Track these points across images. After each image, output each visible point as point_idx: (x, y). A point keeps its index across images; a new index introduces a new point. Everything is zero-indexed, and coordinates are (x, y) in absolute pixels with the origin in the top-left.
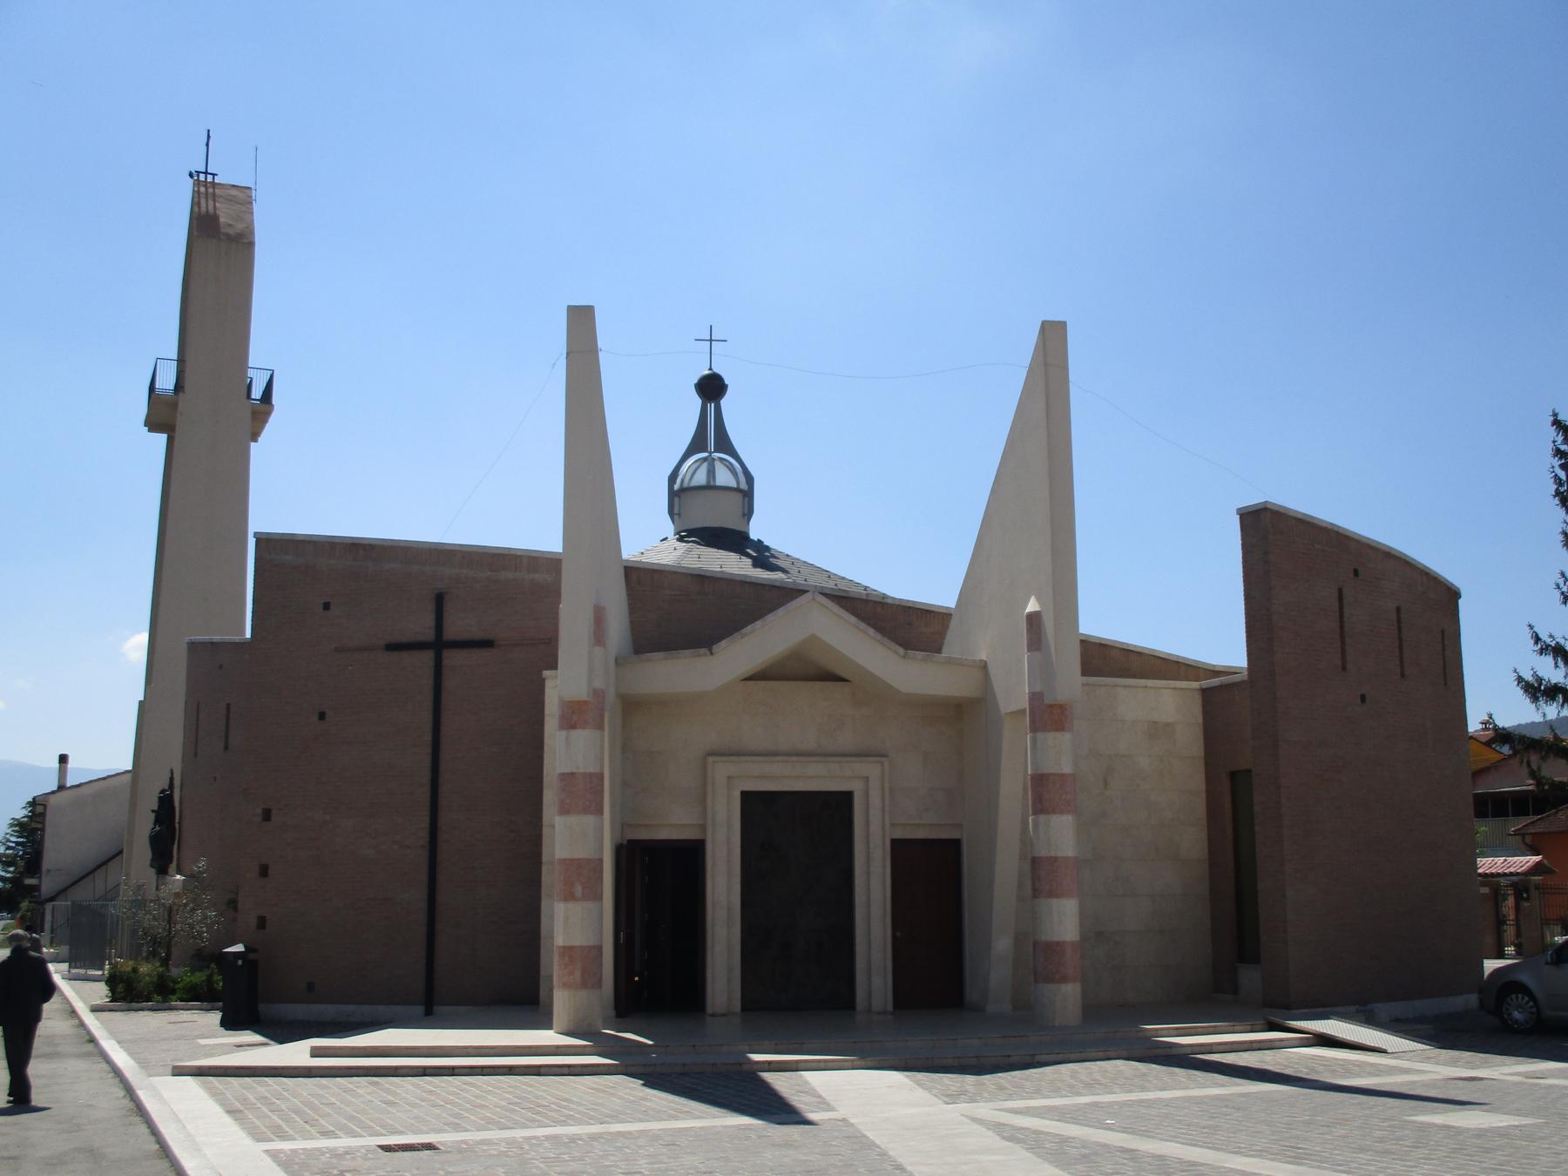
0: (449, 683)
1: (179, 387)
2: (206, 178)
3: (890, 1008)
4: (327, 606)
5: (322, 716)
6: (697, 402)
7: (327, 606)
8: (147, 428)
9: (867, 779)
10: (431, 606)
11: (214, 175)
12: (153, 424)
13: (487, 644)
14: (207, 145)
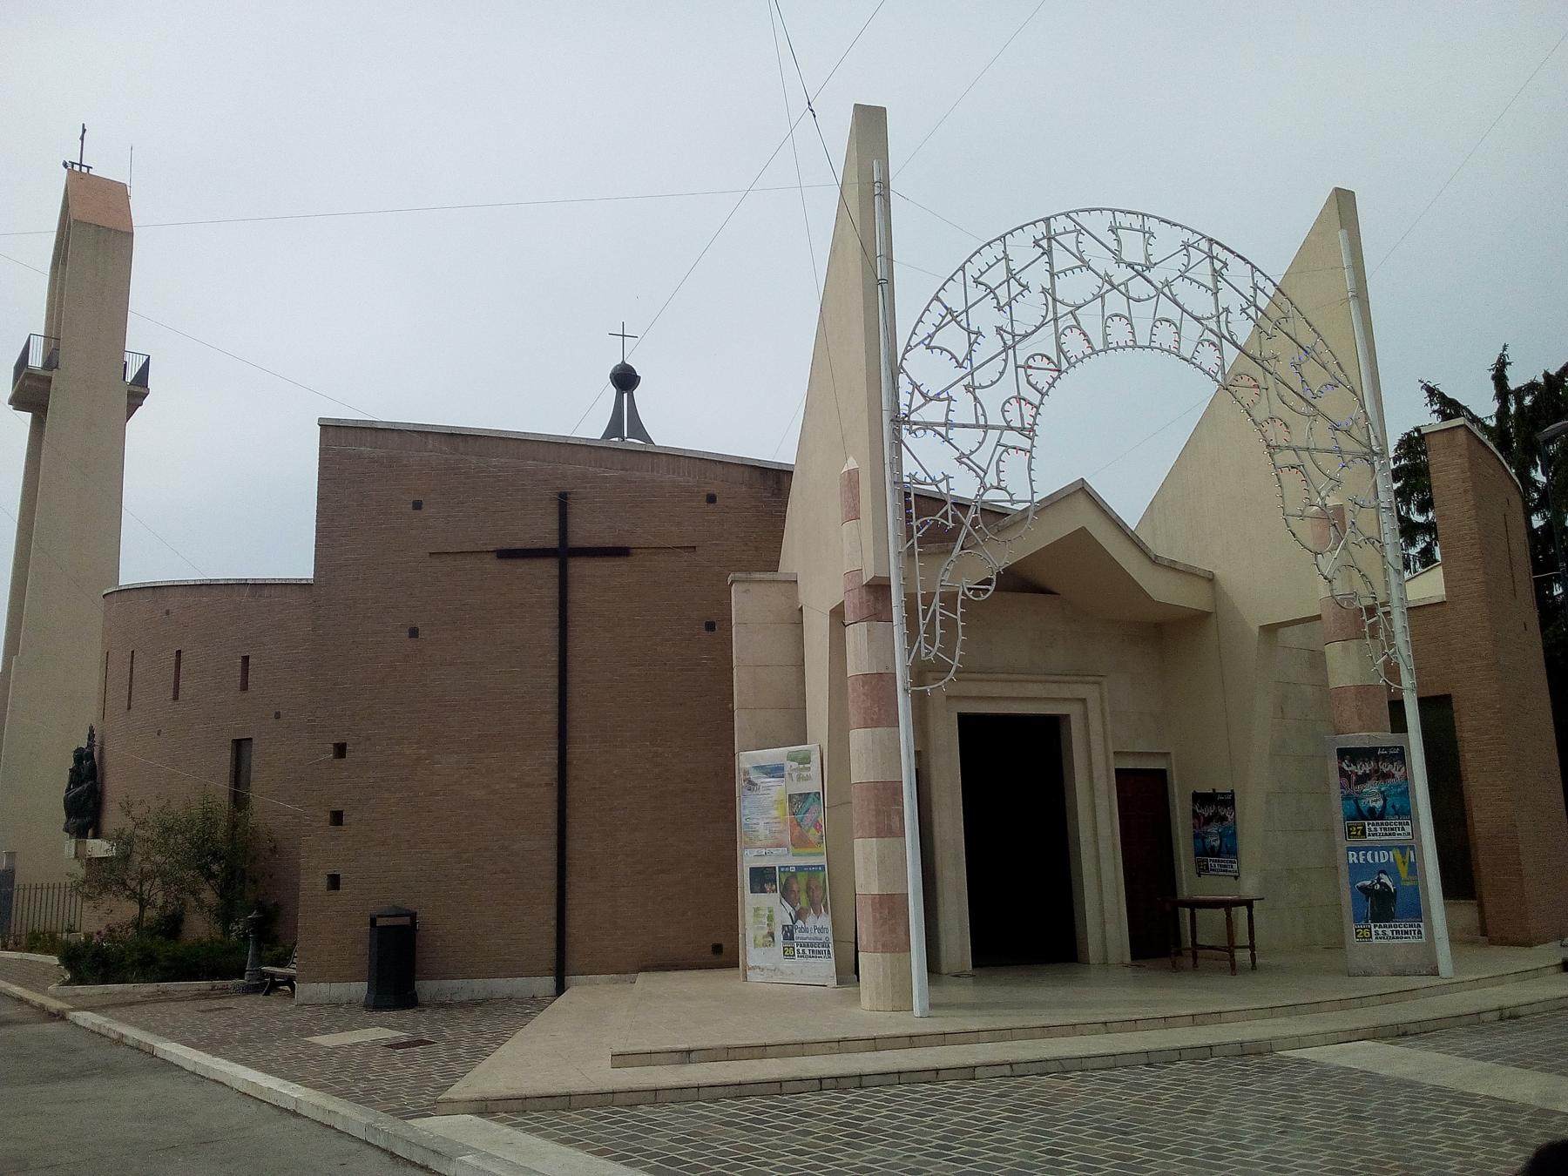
0: (576, 594)
1: (51, 362)
2: (81, 169)
3: (1128, 959)
4: (417, 505)
5: (414, 633)
6: (612, 391)
7: (417, 505)
8: (11, 407)
9: (1084, 701)
10: (554, 507)
11: (89, 168)
12: (18, 402)
13: (621, 552)
14: (82, 139)
